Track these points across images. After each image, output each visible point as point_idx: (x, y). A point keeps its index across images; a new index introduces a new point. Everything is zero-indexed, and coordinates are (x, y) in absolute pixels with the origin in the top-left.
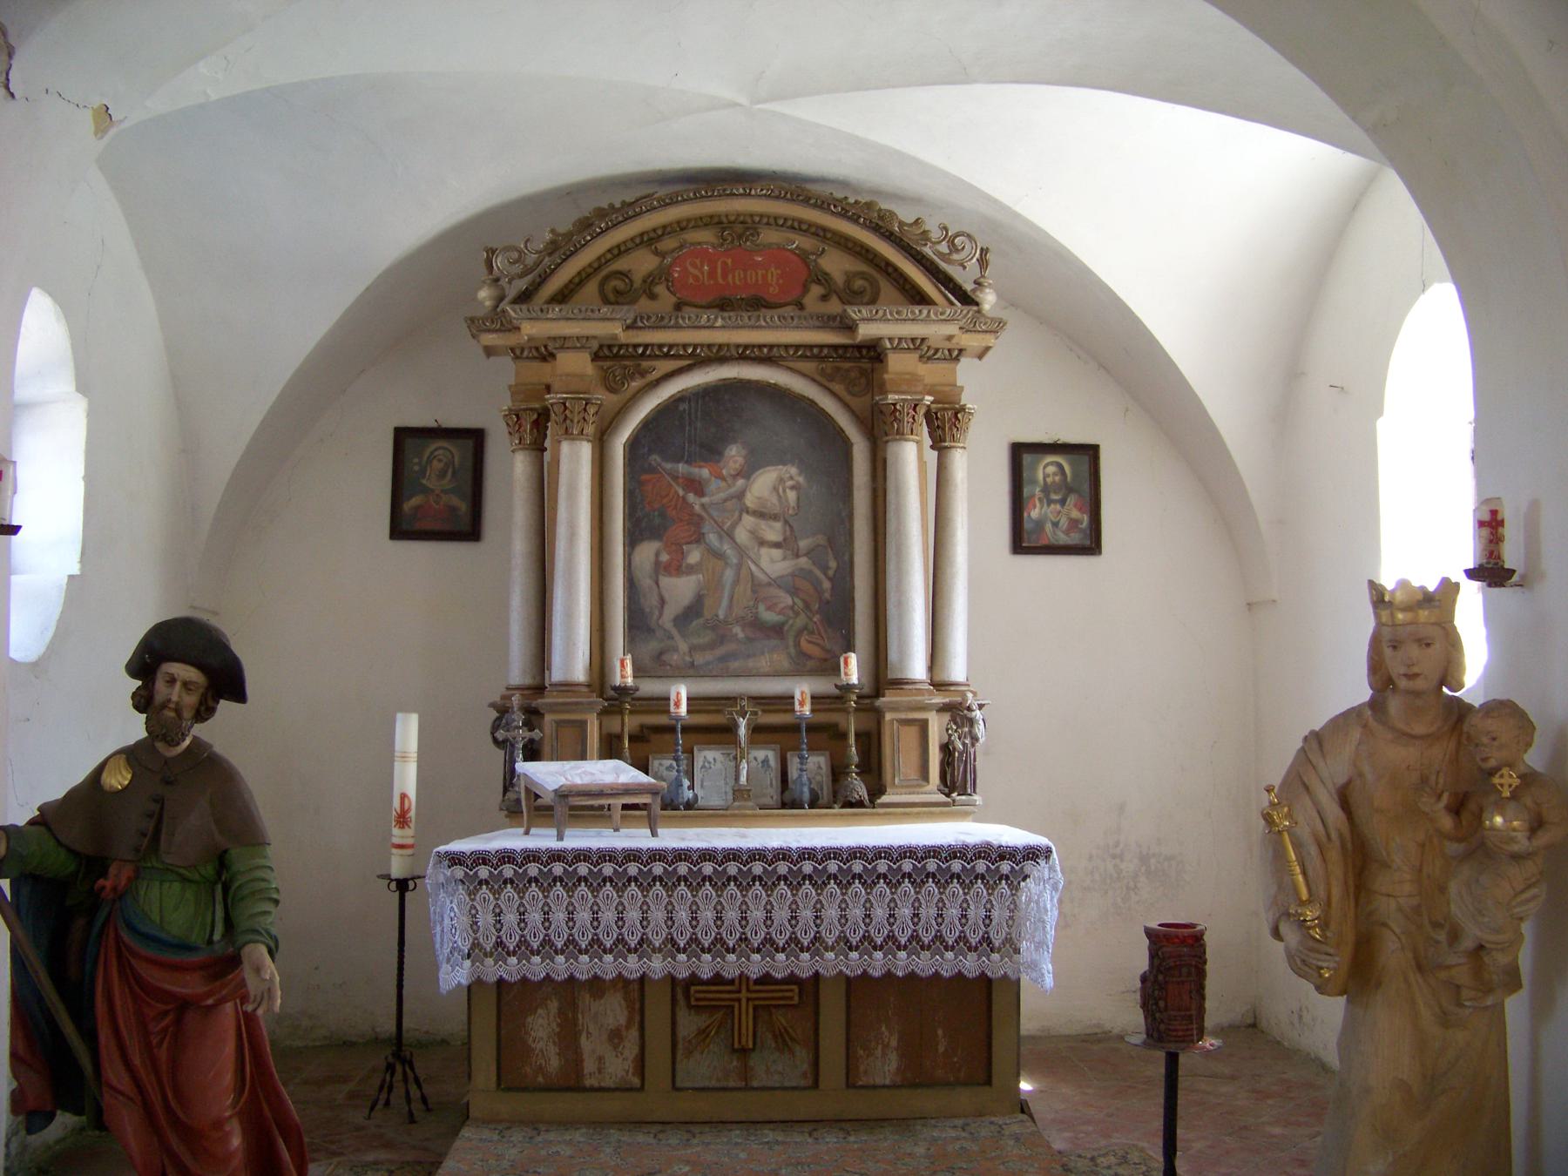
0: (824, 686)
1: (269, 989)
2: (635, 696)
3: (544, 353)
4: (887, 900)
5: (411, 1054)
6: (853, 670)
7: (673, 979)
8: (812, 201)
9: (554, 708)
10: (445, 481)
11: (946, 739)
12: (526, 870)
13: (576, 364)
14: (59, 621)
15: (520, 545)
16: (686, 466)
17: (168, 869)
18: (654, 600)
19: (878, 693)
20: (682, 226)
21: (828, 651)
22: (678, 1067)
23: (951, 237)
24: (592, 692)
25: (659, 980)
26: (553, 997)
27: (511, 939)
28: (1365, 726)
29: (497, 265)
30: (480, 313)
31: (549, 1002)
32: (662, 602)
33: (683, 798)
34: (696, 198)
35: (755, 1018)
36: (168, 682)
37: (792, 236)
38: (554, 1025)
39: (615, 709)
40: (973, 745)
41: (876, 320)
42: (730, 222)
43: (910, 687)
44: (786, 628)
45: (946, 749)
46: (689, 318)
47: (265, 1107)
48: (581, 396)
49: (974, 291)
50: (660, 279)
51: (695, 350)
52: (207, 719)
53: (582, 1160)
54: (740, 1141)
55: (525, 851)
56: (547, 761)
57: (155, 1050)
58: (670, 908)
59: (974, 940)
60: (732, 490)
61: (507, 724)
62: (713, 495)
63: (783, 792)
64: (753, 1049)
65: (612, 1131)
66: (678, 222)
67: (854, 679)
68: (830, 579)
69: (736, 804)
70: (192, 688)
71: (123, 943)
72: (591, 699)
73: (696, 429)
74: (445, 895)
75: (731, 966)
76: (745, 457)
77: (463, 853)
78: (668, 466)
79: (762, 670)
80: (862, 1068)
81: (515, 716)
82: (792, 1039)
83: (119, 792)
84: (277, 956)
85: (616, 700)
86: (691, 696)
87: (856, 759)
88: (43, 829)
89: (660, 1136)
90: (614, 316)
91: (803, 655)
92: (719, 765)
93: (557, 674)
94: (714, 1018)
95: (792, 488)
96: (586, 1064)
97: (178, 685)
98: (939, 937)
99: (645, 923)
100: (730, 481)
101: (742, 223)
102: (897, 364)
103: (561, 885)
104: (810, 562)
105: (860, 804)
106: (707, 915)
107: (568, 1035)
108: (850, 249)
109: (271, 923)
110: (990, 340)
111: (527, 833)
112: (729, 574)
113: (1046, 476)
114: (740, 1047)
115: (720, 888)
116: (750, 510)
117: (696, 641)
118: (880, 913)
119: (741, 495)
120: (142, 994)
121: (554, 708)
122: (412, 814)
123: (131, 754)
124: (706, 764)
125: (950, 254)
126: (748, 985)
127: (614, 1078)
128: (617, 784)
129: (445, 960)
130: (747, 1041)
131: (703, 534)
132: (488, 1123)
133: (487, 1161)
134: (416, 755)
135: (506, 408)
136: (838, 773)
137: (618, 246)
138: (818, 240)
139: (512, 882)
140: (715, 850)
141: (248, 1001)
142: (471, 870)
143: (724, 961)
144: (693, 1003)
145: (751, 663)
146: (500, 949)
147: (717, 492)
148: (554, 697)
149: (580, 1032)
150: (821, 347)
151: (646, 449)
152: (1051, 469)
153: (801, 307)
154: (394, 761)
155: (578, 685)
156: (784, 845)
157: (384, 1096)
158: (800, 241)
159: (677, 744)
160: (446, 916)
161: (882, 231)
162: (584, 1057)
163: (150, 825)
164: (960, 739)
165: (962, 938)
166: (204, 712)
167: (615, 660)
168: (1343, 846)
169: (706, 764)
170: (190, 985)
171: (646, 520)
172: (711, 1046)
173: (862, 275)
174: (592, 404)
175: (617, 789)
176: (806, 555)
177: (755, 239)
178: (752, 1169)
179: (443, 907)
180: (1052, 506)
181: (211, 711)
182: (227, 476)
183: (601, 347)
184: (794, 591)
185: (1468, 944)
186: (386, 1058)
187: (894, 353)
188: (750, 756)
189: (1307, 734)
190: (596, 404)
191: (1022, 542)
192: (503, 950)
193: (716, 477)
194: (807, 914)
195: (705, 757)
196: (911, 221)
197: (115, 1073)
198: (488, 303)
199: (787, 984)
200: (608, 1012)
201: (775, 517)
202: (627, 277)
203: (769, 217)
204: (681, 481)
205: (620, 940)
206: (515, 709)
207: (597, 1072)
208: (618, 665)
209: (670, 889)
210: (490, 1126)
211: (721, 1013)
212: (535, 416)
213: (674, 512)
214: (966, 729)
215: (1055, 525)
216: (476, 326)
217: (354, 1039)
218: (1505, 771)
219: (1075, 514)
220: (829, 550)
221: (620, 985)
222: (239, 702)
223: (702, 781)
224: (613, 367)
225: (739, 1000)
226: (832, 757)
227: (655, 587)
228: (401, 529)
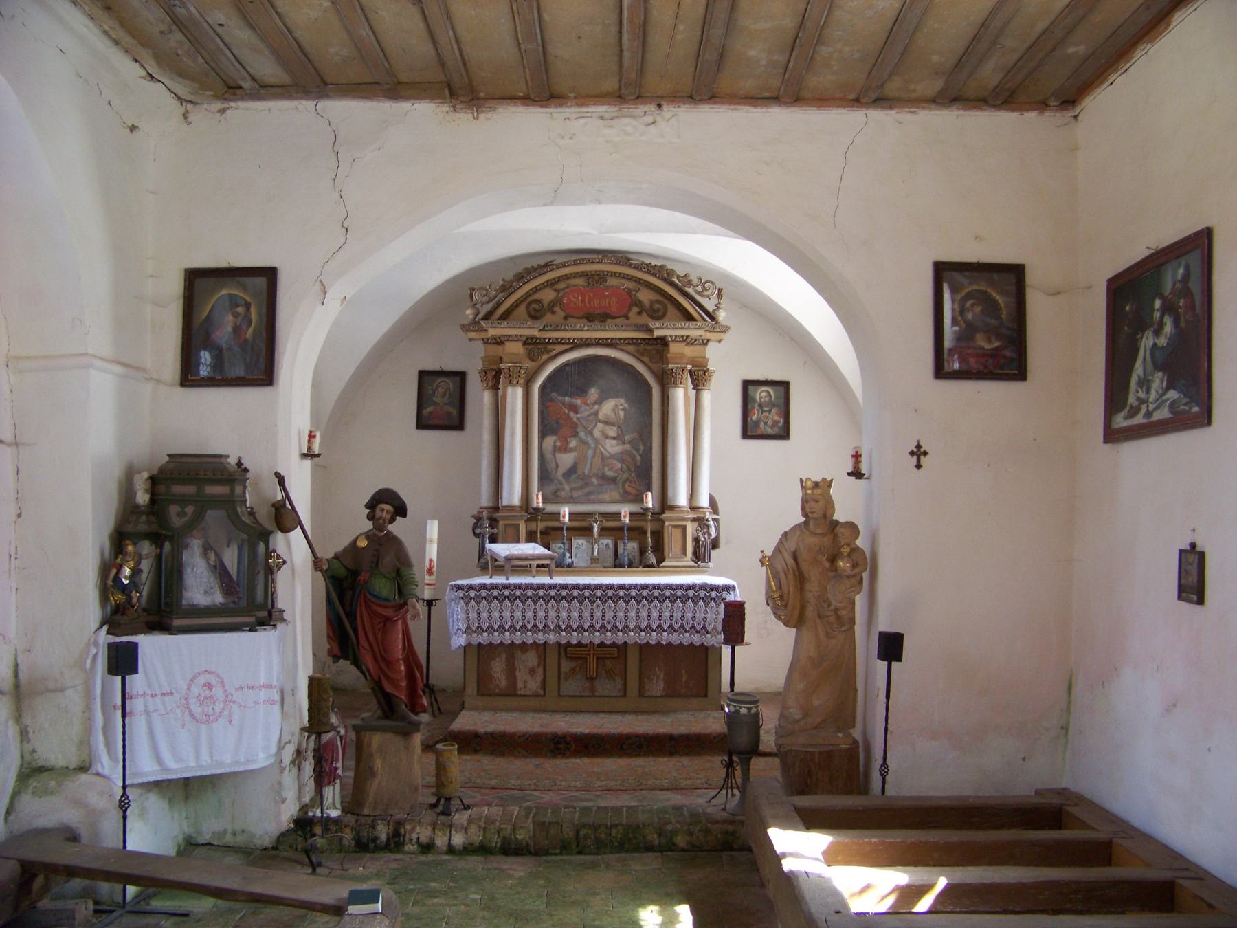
0: (635, 508)
3: (499, 341)
4: (658, 609)
6: (650, 501)
8: (633, 266)
9: (504, 518)
11: (696, 536)
13: (516, 348)
15: (487, 437)
16: (570, 399)
19: (663, 512)
20: (568, 277)
21: (638, 491)
24: (522, 510)
25: (553, 644)
28: (801, 530)
30: (466, 322)
32: (557, 466)
34: (575, 264)
35: (597, 664)
37: (623, 281)
38: (504, 666)
42: (592, 275)
44: (618, 479)
45: (696, 540)
49: (714, 311)
59: (699, 628)
60: (592, 411)
61: (481, 525)
63: (615, 560)
66: (566, 275)
67: (650, 505)
68: (641, 455)
69: (592, 565)
75: (586, 638)
78: (560, 398)
80: (647, 688)
82: (614, 674)
85: (533, 514)
86: (572, 512)
87: (651, 544)
91: (625, 492)
93: (505, 502)
95: (622, 410)
98: (682, 626)
99: (546, 618)
102: (674, 348)
105: (652, 566)
106: (575, 614)
107: (511, 670)
110: (721, 336)
112: (590, 453)
117: (574, 485)
118: (655, 614)
119: (596, 413)
121: (504, 518)
122: (435, 569)
123: (368, 536)
136: (642, 551)
144: (568, 655)
145: (601, 497)
147: (585, 411)
149: (516, 669)
150: (637, 339)
152: (764, 394)
153: (627, 318)
156: (611, 583)
158: (628, 284)
165: (693, 627)
166: (392, 520)
168: (794, 574)
170: (389, 612)
173: (657, 301)
176: (629, 443)
179: (453, 610)
180: (764, 414)
181: (394, 520)
182: (336, 398)
183: (527, 339)
184: (622, 461)
185: (832, 607)
189: (787, 530)
191: (749, 431)
194: (621, 614)
197: (363, 642)
198: (471, 317)
199: (612, 647)
201: (613, 424)
203: (611, 272)
208: (535, 497)
209: (558, 602)
212: (494, 373)
214: (705, 530)
215: (765, 423)
216: (465, 328)
218: (845, 547)
219: (776, 418)
223: (576, 555)
225: (589, 655)
226: (640, 543)
228: (422, 424)
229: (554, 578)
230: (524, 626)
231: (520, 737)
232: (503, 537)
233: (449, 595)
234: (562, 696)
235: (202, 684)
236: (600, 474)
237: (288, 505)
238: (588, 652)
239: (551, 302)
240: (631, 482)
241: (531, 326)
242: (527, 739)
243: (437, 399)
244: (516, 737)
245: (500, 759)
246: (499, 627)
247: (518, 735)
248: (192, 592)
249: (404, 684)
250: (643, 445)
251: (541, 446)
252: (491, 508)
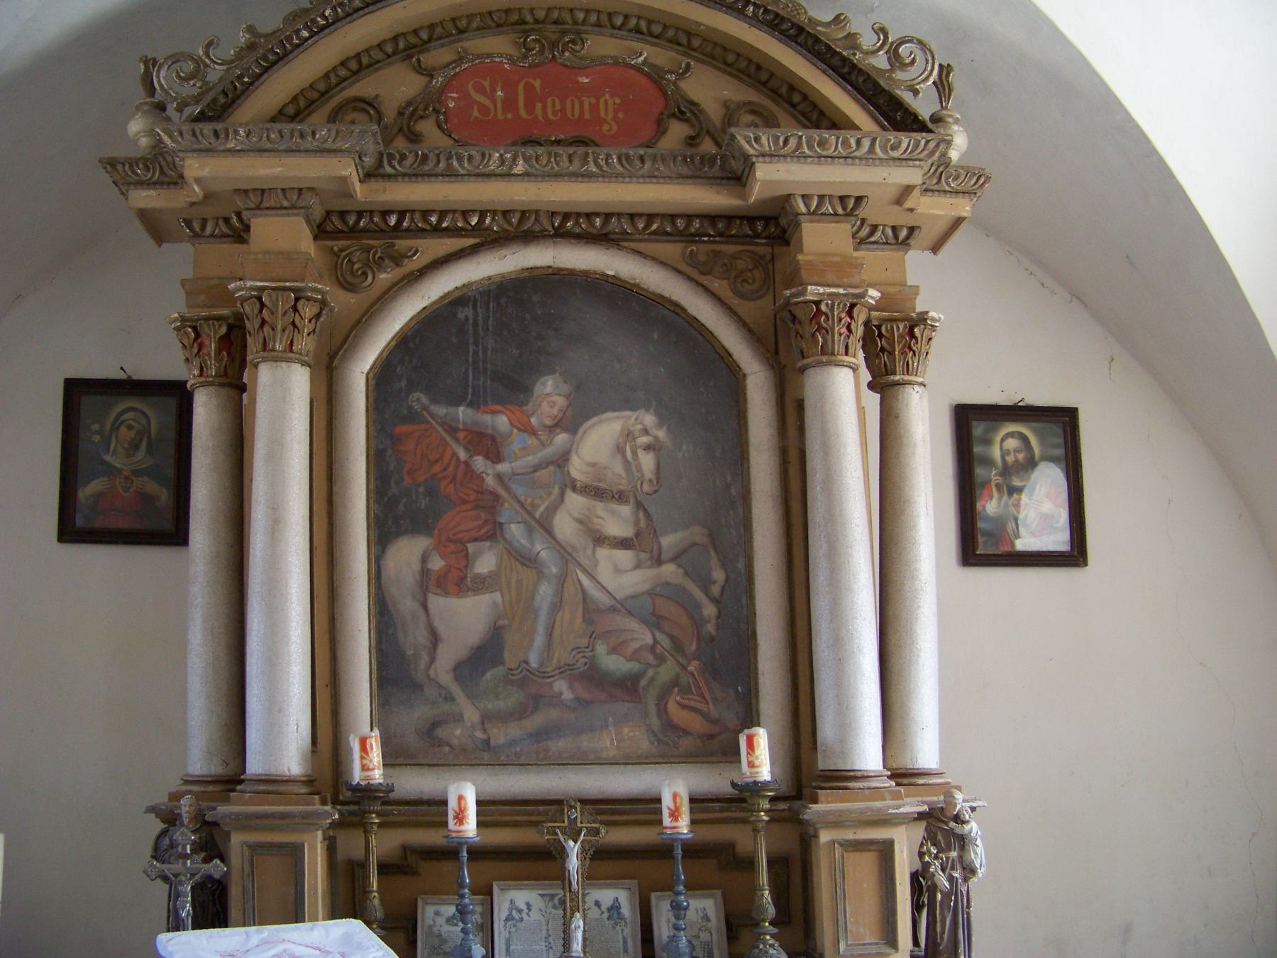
0: (713, 780)
9: (246, 822)
10: (141, 454)
16: (470, 411)
18: (420, 636)
23: (892, 43)
29: (159, 82)
30: (121, 152)
32: (435, 638)
37: (637, 46)
39: (355, 819)
40: (966, 880)
41: (784, 156)
42: (537, 21)
43: (860, 784)
44: (643, 683)
46: (470, 158)
48: (287, 284)
50: (426, 109)
51: (481, 220)
60: (548, 451)
62: (516, 459)
67: (765, 773)
73: (485, 350)
76: (568, 397)
78: (441, 410)
79: (604, 754)
86: (481, 799)
87: (771, 911)
90: (338, 145)
91: (670, 726)
92: (535, 915)
95: (648, 448)
100: (543, 435)
101: (555, 23)
104: (681, 571)
108: (729, 65)
112: (545, 592)
113: (1004, 453)
116: (578, 485)
119: (561, 461)
124: (514, 913)
125: (892, 70)
131: (501, 524)
135: (176, 315)
137: (358, 56)
138: (678, 52)
145: (585, 743)
148: (246, 803)
151: (404, 383)
152: (1012, 443)
155: (287, 781)
158: (646, 53)
159: (462, 886)
161: (784, 27)
164: (943, 870)
167: (351, 738)
169: (514, 913)
174: (308, 299)
176: (674, 559)
177: (578, 48)
184: (655, 621)
187: (812, 222)
188: (587, 899)
190: (316, 300)
193: (520, 430)
195: (512, 902)
196: (828, 17)
201: (620, 497)
202: (373, 107)
204: (461, 435)
212: (224, 330)
213: (451, 488)
214: (954, 854)
220: (713, 554)
223: (508, 942)
224: (348, 247)
227: (421, 612)
228: (70, 531)
236: (581, 666)
239: (409, 103)
240: (685, 691)
241: (329, 145)
250: (724, 567)
252: (216, 781)
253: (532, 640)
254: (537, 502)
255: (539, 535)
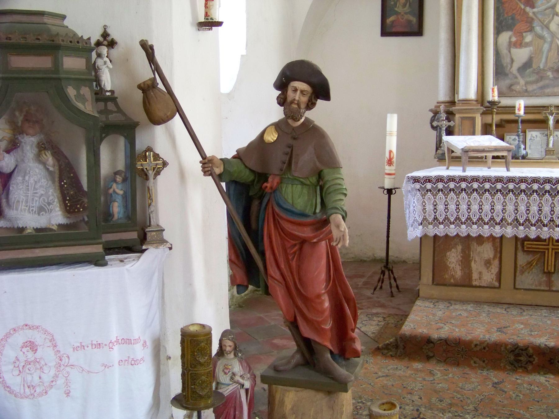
1: (343, 235)
2: (499, 105)
5: (392, 267)
7: (516, 238)
9: (460, 111)
10: (405, 9)
12: (448, 185)
14: (238, 75)
15: (444, 36)
17: (295, 179)
22: (517, 279)
24: (478, 104)
25: (510, 238)
26: (459, 244)
27: (441, 216)
31: (457, 246)
32: (512, 61)
33: (521, 154)
36: (293, 91)
38: (459, 257)
47: (339, 289)
52: (312, 108)
53: (472, 318)
54: (546, 315)
55: (448, 176)
56: (457, 135)
57: (291, 262)
58: (516, 204)
61: (438, 119)
62: (539, 7)
64: (554, 273)
65: (485, 306)
70: (305, 93)
71: (276, 212)
72: (478, 107)
74: (411, 196)
77: (420, 177)
81: (442, 115)
83: (272, 143)
84: (346, 220)
85: (489, 107)
88: (239, 160)
89: (508, 310)
92: (538, 139)
93: (461, 95)
94: (535, 257)
96: (473, 275)
97: (299, 92)
99: (504, 211)
103: (453, 192)
107: (466, 261)
109: (343, 205)
111: (448, 169)
112: (546, 46)
114: (547, 271)
115: (541, 196)
120: (285, 236)
121: (460, 111)
122: (394, 160)
123: (277, 126)
126: (553, 241)
127: (486, 282)
128: (491, 146)
129: (410, 226)
130: (551, 268)
131: (534, 27)
132: (428, 299)
133: (429, 316)
134: (396, 133)
139: (442, 190)
140: (539, 178)
141: (333, 241)
142: (423, 185)
143: (542, 230)
144: (525, 249)
146: (436, 221)
148: (460, 106)
149: (471, 261)
154: (386, 136)
155: (470, 100)
157: (380, 284)
159: (518, 128)
160: (411, 205)
162: (473, 272)
163: (287, 158)
166: (310, 105)
167: (489, 88)
170: (306, 233)
171: (505, 21)
172: (533, 269)
175: (491, 149)
178: (554, 329)
181: (314, 104)
186: (381, 268)
192: (437, 221)
197: (273, 271)
200: (485, 252)
205: (492, 219)
206: (442, 112)
207: (478, 279)
208: (491, 91)
210: (429, 301)
211: (539, 255)
217: (365, 259)
221: (491, 239)
222: (327, 100)
223: (530, 146)
225: (548, 249)
227: (508, 53)
228: (385, 32)
229: (511, 169)
230: (481, 219)
231: (476, 345)
232: (459, 129)
233: (406, 187)
234: (517, 289)
235: (21, 344)
237: (161, 86)
238: (547, 247)
242: (484, 348)
243: (399, 9)
244: (473, 346)
245: (455, 369)
246: (455, 220)
247: (475, 343)
248: (17, 209)
249: (328, 326)
251: (496, 42)
252: (448, 102)
253: (541, 61)
254: (545, 20)
255: (545, 29)
